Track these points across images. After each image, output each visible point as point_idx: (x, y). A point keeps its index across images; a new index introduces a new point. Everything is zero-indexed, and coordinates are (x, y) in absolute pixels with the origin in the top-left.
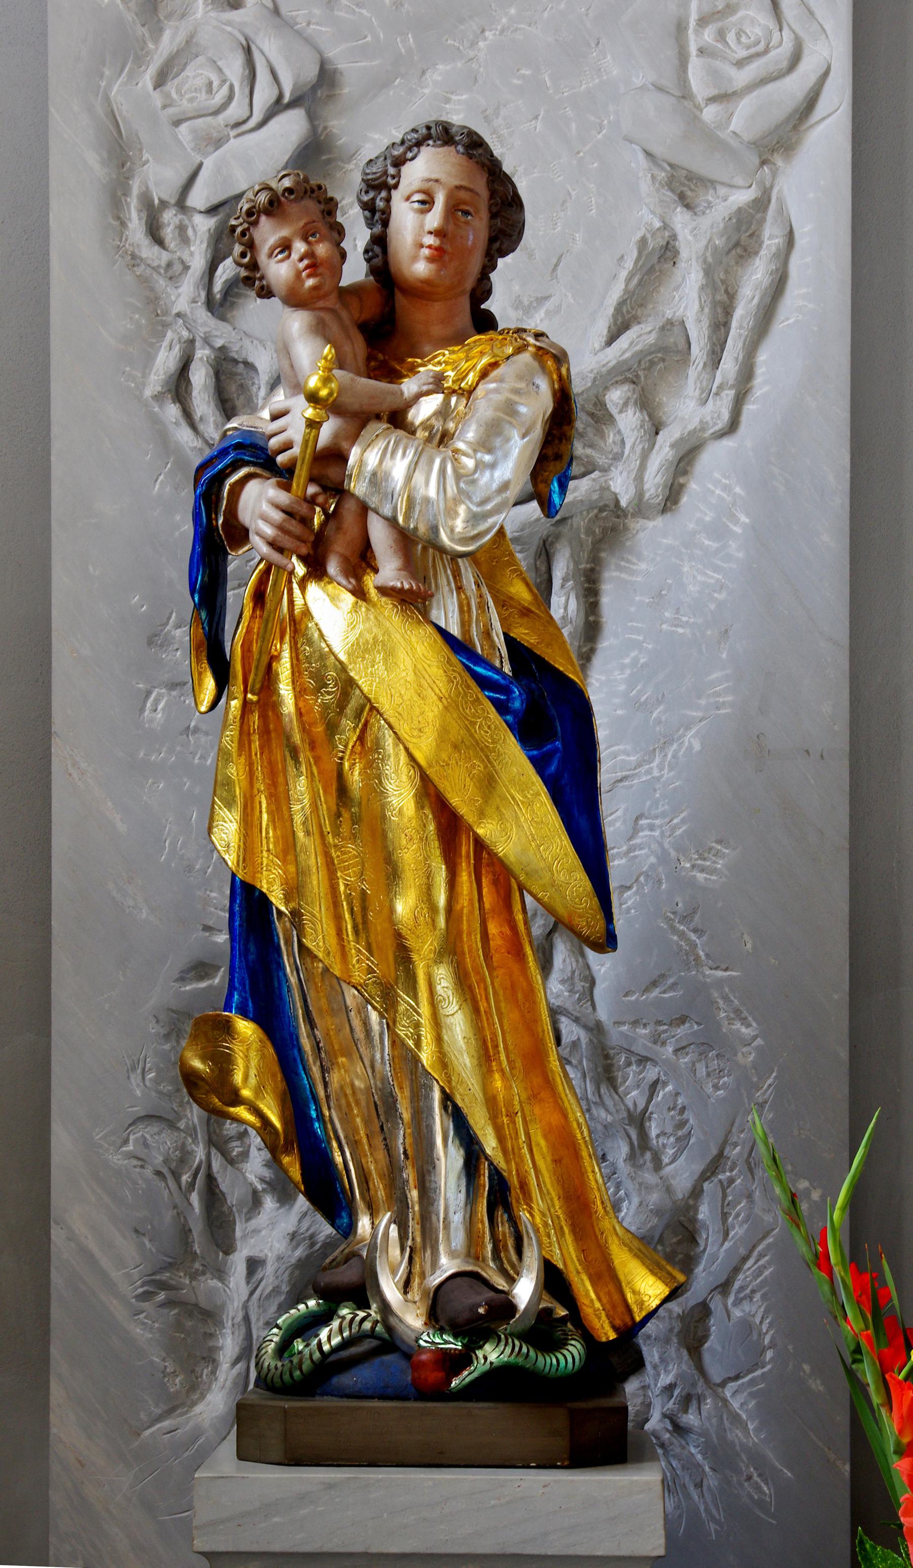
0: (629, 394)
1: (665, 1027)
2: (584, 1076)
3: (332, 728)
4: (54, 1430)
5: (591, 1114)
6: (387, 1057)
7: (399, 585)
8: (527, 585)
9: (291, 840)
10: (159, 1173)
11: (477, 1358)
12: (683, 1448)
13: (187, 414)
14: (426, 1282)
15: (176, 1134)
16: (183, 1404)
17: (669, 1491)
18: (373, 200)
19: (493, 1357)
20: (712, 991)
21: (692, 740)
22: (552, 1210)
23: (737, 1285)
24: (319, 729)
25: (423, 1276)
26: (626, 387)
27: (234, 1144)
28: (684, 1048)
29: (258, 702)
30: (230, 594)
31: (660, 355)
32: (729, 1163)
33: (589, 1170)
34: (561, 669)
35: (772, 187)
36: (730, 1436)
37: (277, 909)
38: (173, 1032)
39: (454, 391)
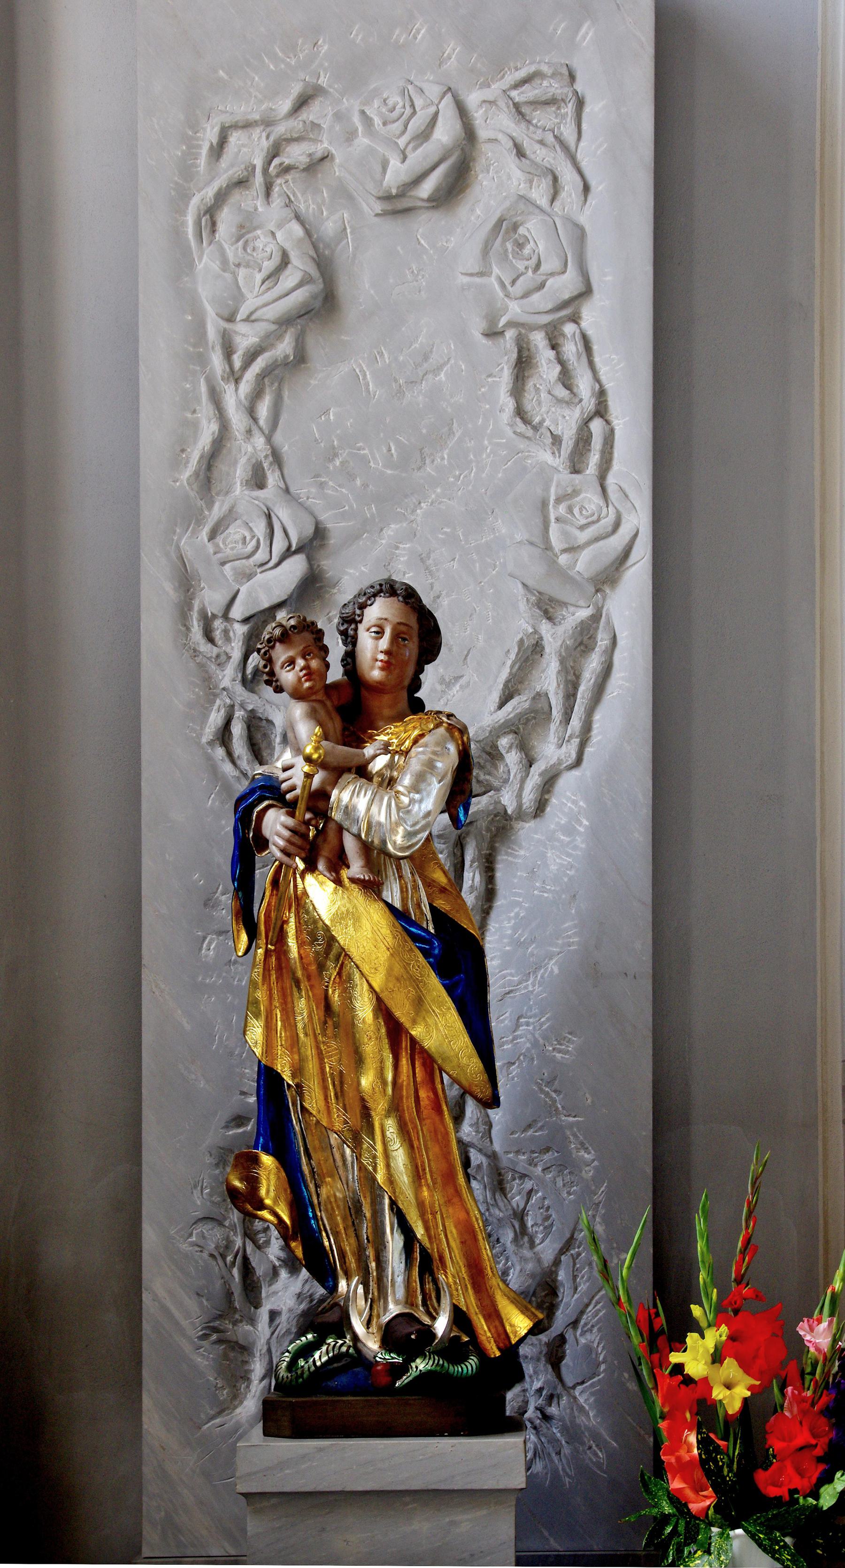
0: (513, 741)
1: (537, 1155)
2: (485, 1187)
3: (321, 967)
4: (145, 1426)
5: (489, 1213)
6: (356, 1178)
7: (362, 877)
8: (444, 872)
9: (296, 1038)
10: (212, 1256)
11: (412, 1368)
12: (548, 1429)
13: (230, 754)
14: (380, 1320)
15: (223, 1229)
16: (228, 1408)
17: (540, 1457)
18: (347, 629)
19: (421, 1367)
20: (566, 1131)
21: (553, 967)
22: (460, 1274)
23: (582, 1322)
24: (313, 968)
25: (379, 1316)
26: (511, 736)
27: (261, 1235)
28: (548, 1168)
29: (274, 950)
30: (257, 872)
31: (532, 715)
32: (577, 1243)
33: (483, 1248)
34: (465, 927)
35: (603, 607)
36: (578, 1421)
37: (287, 1083)
38: (221, 1162)
39: (397, 752)
